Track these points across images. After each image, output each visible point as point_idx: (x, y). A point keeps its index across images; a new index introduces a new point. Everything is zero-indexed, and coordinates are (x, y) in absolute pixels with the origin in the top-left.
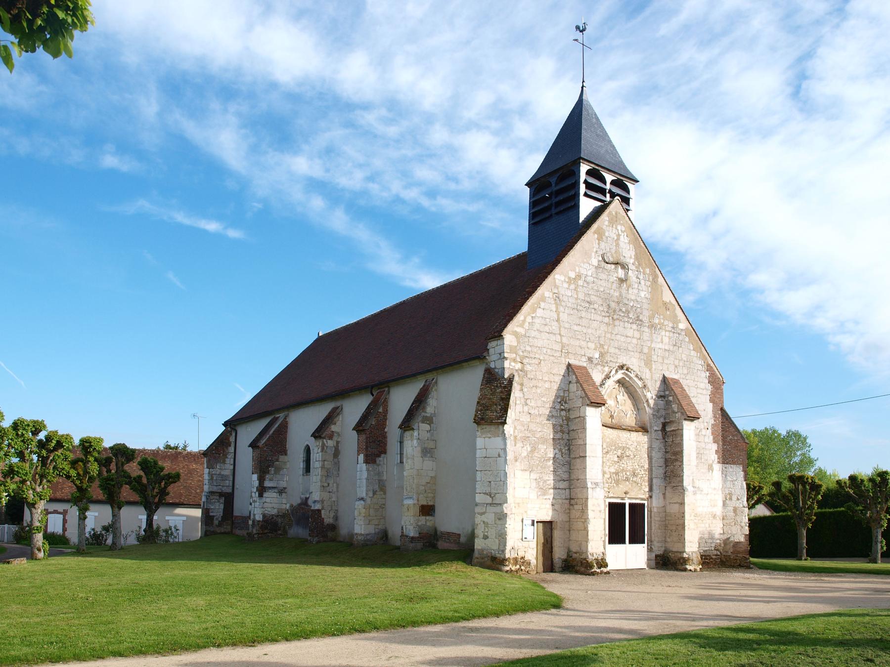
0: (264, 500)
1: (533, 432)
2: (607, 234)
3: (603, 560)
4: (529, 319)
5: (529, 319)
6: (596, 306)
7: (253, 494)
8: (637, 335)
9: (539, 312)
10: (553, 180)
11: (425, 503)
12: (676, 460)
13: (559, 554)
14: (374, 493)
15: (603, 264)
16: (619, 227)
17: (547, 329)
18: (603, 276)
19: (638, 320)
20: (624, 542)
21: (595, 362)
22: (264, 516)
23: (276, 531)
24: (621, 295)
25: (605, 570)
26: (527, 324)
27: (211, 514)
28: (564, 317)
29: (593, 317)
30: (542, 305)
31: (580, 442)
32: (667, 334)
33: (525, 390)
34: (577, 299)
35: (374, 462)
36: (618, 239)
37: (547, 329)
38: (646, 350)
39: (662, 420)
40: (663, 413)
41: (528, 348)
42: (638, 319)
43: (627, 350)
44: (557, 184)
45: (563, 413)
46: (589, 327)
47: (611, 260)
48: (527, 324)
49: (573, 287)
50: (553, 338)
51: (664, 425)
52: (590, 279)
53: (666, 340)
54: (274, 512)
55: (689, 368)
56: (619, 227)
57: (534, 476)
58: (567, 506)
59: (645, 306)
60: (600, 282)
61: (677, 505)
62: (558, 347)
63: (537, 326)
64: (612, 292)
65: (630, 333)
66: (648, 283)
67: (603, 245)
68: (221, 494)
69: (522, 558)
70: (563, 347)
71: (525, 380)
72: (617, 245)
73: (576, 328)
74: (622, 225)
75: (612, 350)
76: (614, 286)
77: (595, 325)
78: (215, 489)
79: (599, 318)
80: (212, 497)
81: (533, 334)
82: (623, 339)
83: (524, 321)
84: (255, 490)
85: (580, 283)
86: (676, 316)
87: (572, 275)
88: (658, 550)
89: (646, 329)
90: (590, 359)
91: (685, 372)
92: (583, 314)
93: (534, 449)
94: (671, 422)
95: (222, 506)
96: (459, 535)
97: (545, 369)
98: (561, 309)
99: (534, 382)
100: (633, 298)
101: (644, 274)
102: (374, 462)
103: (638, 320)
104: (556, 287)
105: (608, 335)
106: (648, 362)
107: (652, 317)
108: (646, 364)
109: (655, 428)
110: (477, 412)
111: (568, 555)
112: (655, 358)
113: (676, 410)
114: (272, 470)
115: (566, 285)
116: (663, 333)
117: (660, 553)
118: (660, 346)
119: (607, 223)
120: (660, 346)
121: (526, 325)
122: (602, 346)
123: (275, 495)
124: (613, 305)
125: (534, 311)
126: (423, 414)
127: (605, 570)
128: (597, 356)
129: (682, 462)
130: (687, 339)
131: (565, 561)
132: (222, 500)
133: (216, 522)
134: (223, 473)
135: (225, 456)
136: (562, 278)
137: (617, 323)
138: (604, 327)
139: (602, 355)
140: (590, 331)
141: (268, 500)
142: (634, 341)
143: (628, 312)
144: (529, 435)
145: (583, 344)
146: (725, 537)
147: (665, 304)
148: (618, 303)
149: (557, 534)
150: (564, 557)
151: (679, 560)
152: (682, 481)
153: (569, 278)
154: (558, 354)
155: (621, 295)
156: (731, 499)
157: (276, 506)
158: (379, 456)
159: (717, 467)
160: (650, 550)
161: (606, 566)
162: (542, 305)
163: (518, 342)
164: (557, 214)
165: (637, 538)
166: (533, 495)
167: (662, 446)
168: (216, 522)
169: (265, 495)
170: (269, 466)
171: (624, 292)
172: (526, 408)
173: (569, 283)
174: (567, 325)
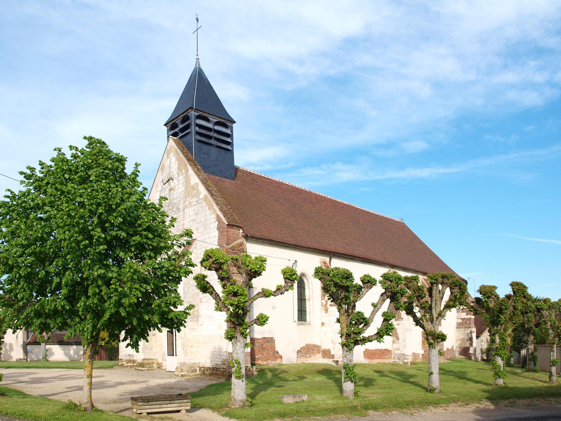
20: (173, 355)
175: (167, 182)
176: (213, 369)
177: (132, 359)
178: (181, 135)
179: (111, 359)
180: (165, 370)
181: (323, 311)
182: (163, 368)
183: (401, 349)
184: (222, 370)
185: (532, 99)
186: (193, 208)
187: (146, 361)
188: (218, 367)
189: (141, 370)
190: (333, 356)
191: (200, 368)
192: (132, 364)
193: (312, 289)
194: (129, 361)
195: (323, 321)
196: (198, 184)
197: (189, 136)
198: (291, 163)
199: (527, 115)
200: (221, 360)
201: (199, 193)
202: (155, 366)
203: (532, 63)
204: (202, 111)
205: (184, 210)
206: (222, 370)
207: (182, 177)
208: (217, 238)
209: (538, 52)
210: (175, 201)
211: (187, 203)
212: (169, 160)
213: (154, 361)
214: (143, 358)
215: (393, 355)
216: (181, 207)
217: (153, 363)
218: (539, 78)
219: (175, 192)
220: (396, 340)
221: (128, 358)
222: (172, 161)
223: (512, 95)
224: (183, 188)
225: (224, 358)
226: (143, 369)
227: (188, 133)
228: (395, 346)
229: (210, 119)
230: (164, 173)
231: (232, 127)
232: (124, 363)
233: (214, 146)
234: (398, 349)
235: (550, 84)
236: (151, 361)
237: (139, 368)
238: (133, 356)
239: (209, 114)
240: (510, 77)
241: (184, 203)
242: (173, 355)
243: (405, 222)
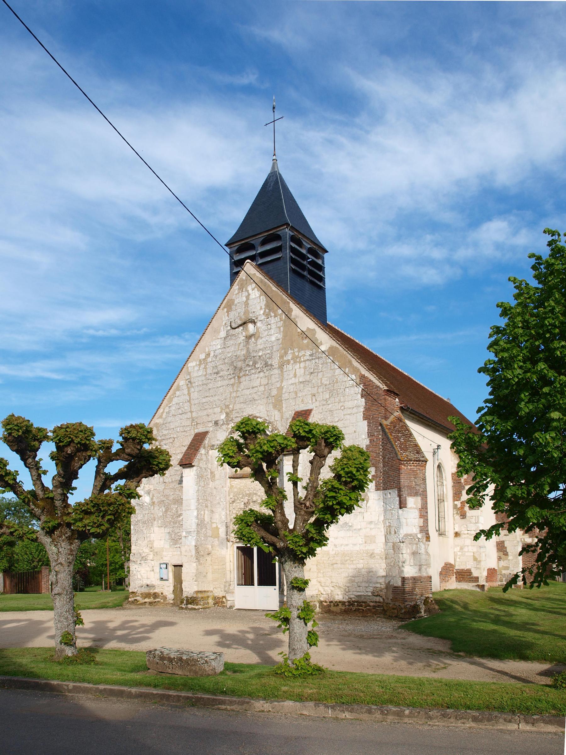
20: (253, 585)
37: (180, 411)
57: (167, 530)
63: (173, 412)
77: (221, 390)
81: (169, 419)
143: (255, 363)
166: (167, 546)
175: (241, 325)
176: (351, 603)
177: (152, 591)
178: (260, 261)
179: (25, 591)
180: (231, 607)
181: (458, 517)
182: (229, 604)
183: (511, 568)
184: (372, 604)
185: (431, 277)
186: (302, 365)
187: (200, 595)
188: (362, 599)
189: (195, 609)
190: (477, 579)
191: (321, 602)
192: (152, 600)
193: (446, 485)
194: (148, 595)
195: (457, 530)
196: (314, 330)
197: (280, 263)
198: (145, 329)
199: (426, 294)
200: (371, 589)
201: (316, 344)
202: (211, 601)
203: (429, 237)
204: (297, 231)
205: (281, 367)
206: (372, 604)
207: (277, 319)
208: (362, 409)
209: (433, 226)
210: (260, 354)
211: (289, 357)
212: (245, 294)
213: (209, 594)
214: (196, 589)
215: (499, 577)
216: (275, 362)
217: (208, 597)
218: (437, 254)
219: (260, 341)
220: (503, 556)
221: (146, 590)
222: (252, 296)
223: (409, 271)
224: (280, 336)
225: (379, 585)
226: (197, 607)
227: (279, 259)
228: (502, 563)
229: (304, 243)
230: (232, 314)
231: (323, 258)
232: (138, 598)
233: (307, 281)
234: (507, 568)
235: (450, 262)
236: (205, 595)
237: (190, 606)
238: (153, 586)
239: (304, 236)
240: (405, 250)
241: (281, 357)
242: (253, 585)
243: (452, 402)
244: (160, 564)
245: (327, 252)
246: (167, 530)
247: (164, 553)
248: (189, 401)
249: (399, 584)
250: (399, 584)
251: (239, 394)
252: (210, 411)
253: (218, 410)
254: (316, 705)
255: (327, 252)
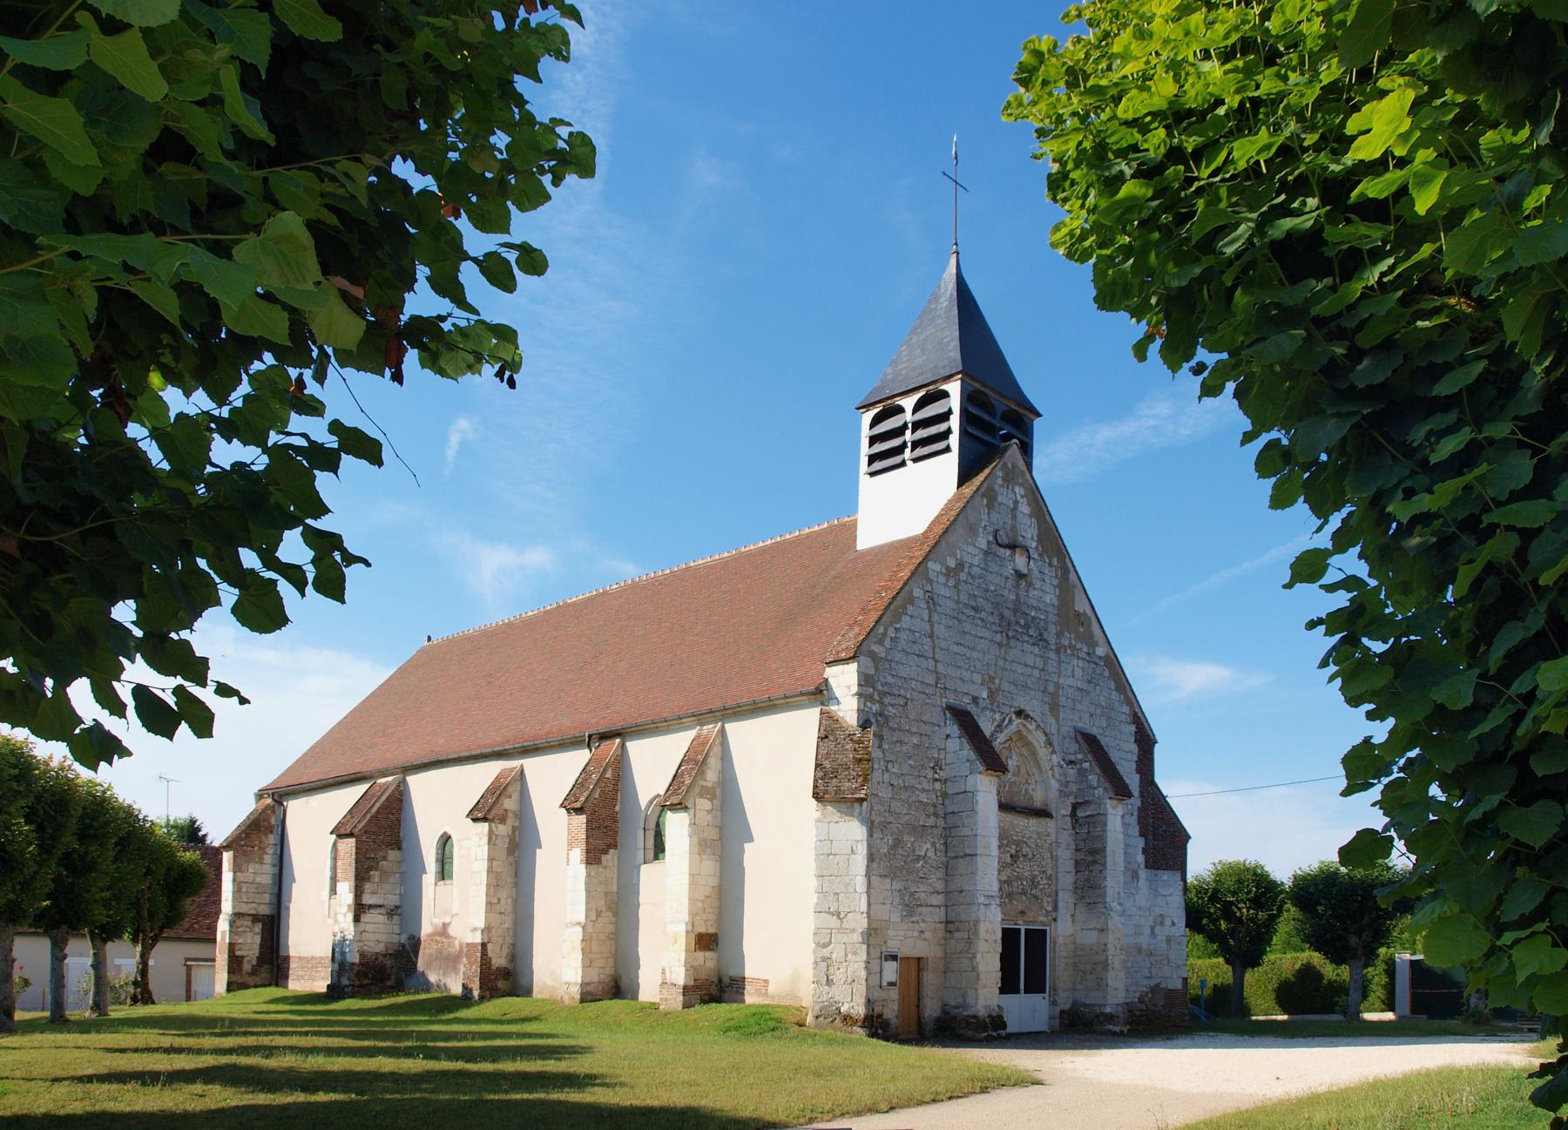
0: (362, 926)
1: (897, 815)
2: (1000, 499)
3: (1000, 1017)
4: (891, 633)
5: (891, 633)
6: (983, 615)
7: (340, 918)
8: (1040, 664)
9: (906, 622)
10: (908, 403)
11: (703, 930)
12: (1094, 862)
13: (931, 1009)
14: (599, 914)
15: (995, 547)
16: (1017, 489)
17: (916, 649)
18: (994, 567)
19: (1041, 640)
20: (1018, 992)
21: (982, 704)
22: (362, 955)
23: (383, 981)
24: (1018, 598)
25: (1003, 1033)
26: (888, 640)
27: (238, 953)
28: (940, 630)
29: (982, 632)
30: (910, 609)
31: (966, 832)
32: (1081, 663)
33: (886, 746)
34: (958, 602)
35: (599, 862)
36: (1015, 509)
37: (916, 649)
38: (1051, 689)
39: (1072, 800)
40: (1074, 788)
41: (890, 680)
42: (1041, 638)
43: (1025, 686)
44: (915, 411)
45: (938, 785)
46: (973, 649)
47: (1006, 541)
48: (888, 640)
49: (951, 583)
50: (924, 663)
51: (1075, 807)
52: (976, 570)
53: (1078, 673)
54: (380, 948)
55: (1109, 718)
56: (1017, 489)
57: (897, 885)
58: (941, 933)
59: (1052, 618)
60: (990, 577)
61: (1094, 934)
62: (930, 679)
63: (902, 644)
64: (1006, 593)
65: (1030, 660)
66: (1055, 582)
67: (994, 516)
68: (256, 918)
69: (880, 1016)
70: (938, 678)
71: (886, 732)
72: (1014, 517)
73: (956, 649)
74: (1020, 485)
75: (1005, 686)
76: (1010, 583)
77: (982, 644)
78: (245, 909)
79: (988, 634)
80: (239, 923)
81: (898, 656)
82: (1020, 669)
83: (885, 634)
84: (344, 909)
85: (963, 576)
86: (1091, 636)
87: (952, 563)
88: (1065, 1003)
89: (1052, 655)
90: (975, 700)
91: (1104, 724)
92: (967, 627)
93: (897, 843)
94: (1086, 802)
95: (258, 939)
96: (766, 981)
97: (913, 715)
98: (936, 618)
99: (896, 736)
100: (1035, 604)
101: (1050, 565)
102: (599, 862)
103: (1041, 640)
104: (930, 581)
105: (1001, 663)
106: (1054, 708)
107: (1059, 635)
108: (1051, 710)
109: (1063, 812)
110: (816, 780)
111: (943, 1011)
112: (1063, 700)
113: (1095, 784)
114: (375, 874)
115: (942, 579)
116: (1075, 662)
117: (1067, 1007)
118: (1070, 681)
119: (999, 481)
120: (1070, 681)
121: (887, 642)
122: (992, 679)
123: (382, 919)
124: (1007, 614)
125: (898, 620)
126: (702, 783)
127: (1003, 1033)
128: (985, 695)
129: (1104, 865)
130: (1107, 673)
131: (938, 1020)
132: (258, 928)
133: (247, 967)
134: (258, 880)
135: (263, 850)
136: (938, 567)
137: (1012, 643)
138: (995, 650)
139: (991, 694)
140: (975, 654)
141: (369, 927)
142: (1036, 673)
143: (1027, 627)
144: (891, 819)
145: (966, 674)
146: (1153, 983)
147: (1078, 615)
148: (1015, 611)
149: (930, 978)
150: (937, 1014)
151: (1098, 1016)
152: (1104, 895)
153: (947, 568)
154: (930, 691)
155: (1018, 598)
156: (1162, 924)
157: (383, 937)
158: (606, 852)
159: (1143, 873)
160: (1054, 1003)
161: (1004, 1026)
162: (910, 609)
163: (877, 669)
164: (915, 460)
165: (1036, 984)
166: (896, 918)
167: (1071, 840)
168: (247, 967)
169: (364, 918)
170: (371, 868)
171: (1022, 594)
172: (886, 775)
173: (947, 576)
174: (943, 644)
244: (187, 959)
245: (1039, 415)
246: (897, 885)
247: (890, 932)
248: (931, 636)
249: (1179, 985)
250: (1179, 985)
251: (1007, 666)
252: (966, 674)
253: (977, 678)
254: (1385, 987)
255: (1039, 415)
